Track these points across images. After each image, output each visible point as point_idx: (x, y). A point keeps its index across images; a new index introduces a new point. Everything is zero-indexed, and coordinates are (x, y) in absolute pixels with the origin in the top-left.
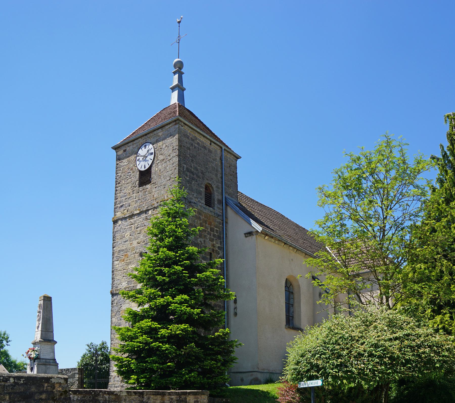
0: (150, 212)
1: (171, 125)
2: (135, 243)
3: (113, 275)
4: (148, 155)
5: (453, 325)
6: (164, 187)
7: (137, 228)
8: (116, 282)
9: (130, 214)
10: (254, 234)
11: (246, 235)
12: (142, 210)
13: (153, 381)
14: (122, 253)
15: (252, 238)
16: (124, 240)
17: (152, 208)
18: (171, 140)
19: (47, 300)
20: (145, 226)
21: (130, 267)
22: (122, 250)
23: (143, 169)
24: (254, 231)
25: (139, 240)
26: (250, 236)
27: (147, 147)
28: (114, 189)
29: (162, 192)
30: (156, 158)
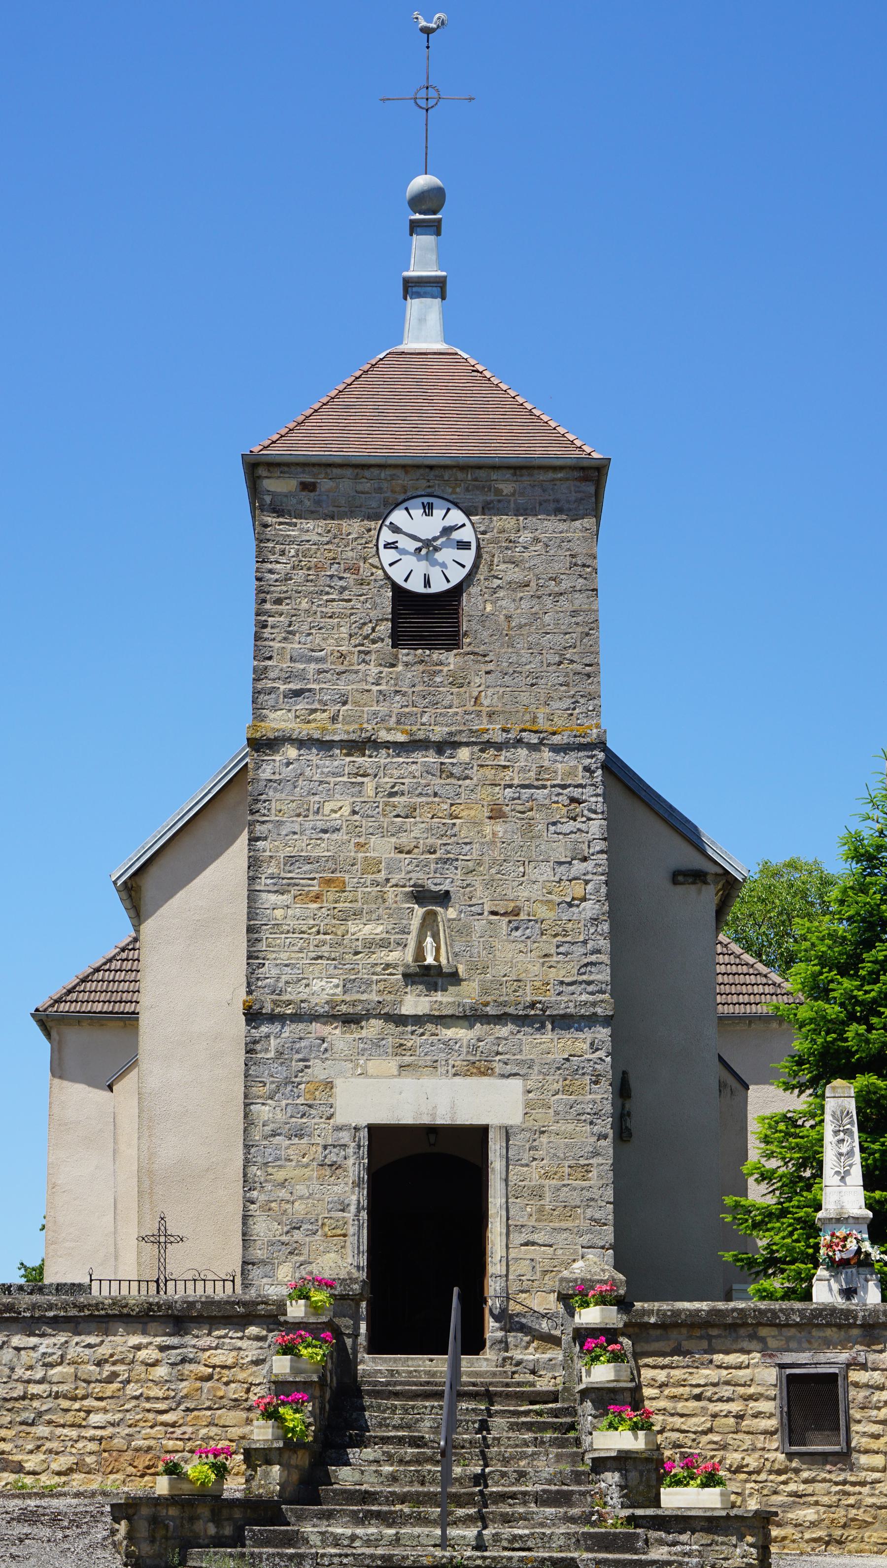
0: (464, 754)
1: (560, 475)
2: (381, 848)
3: (252, 942)
4: (444, 545)
5: (3, 1483)
6: (530, 681)
7: (392, 795)
8: (269, 970)
9: (353, 737)
10: (709, 879)
11: (681, 878)
12: (421, 735)
13: (299, 1356)
14: (307, 867)
15: (699, 892)
16: (320, 825)
17: (475, 743)
18: (563, 526)
19: (721, 1059)
20: (435, 795)
21: (352, 927)
22: (308, 860)
23: (416, 586)
24: (711, 869)
25: (404, 840)
26: (693, 883)
27: (438, 513)
28: (251, 619)
29: (524, 698)
30: (483, 568)
